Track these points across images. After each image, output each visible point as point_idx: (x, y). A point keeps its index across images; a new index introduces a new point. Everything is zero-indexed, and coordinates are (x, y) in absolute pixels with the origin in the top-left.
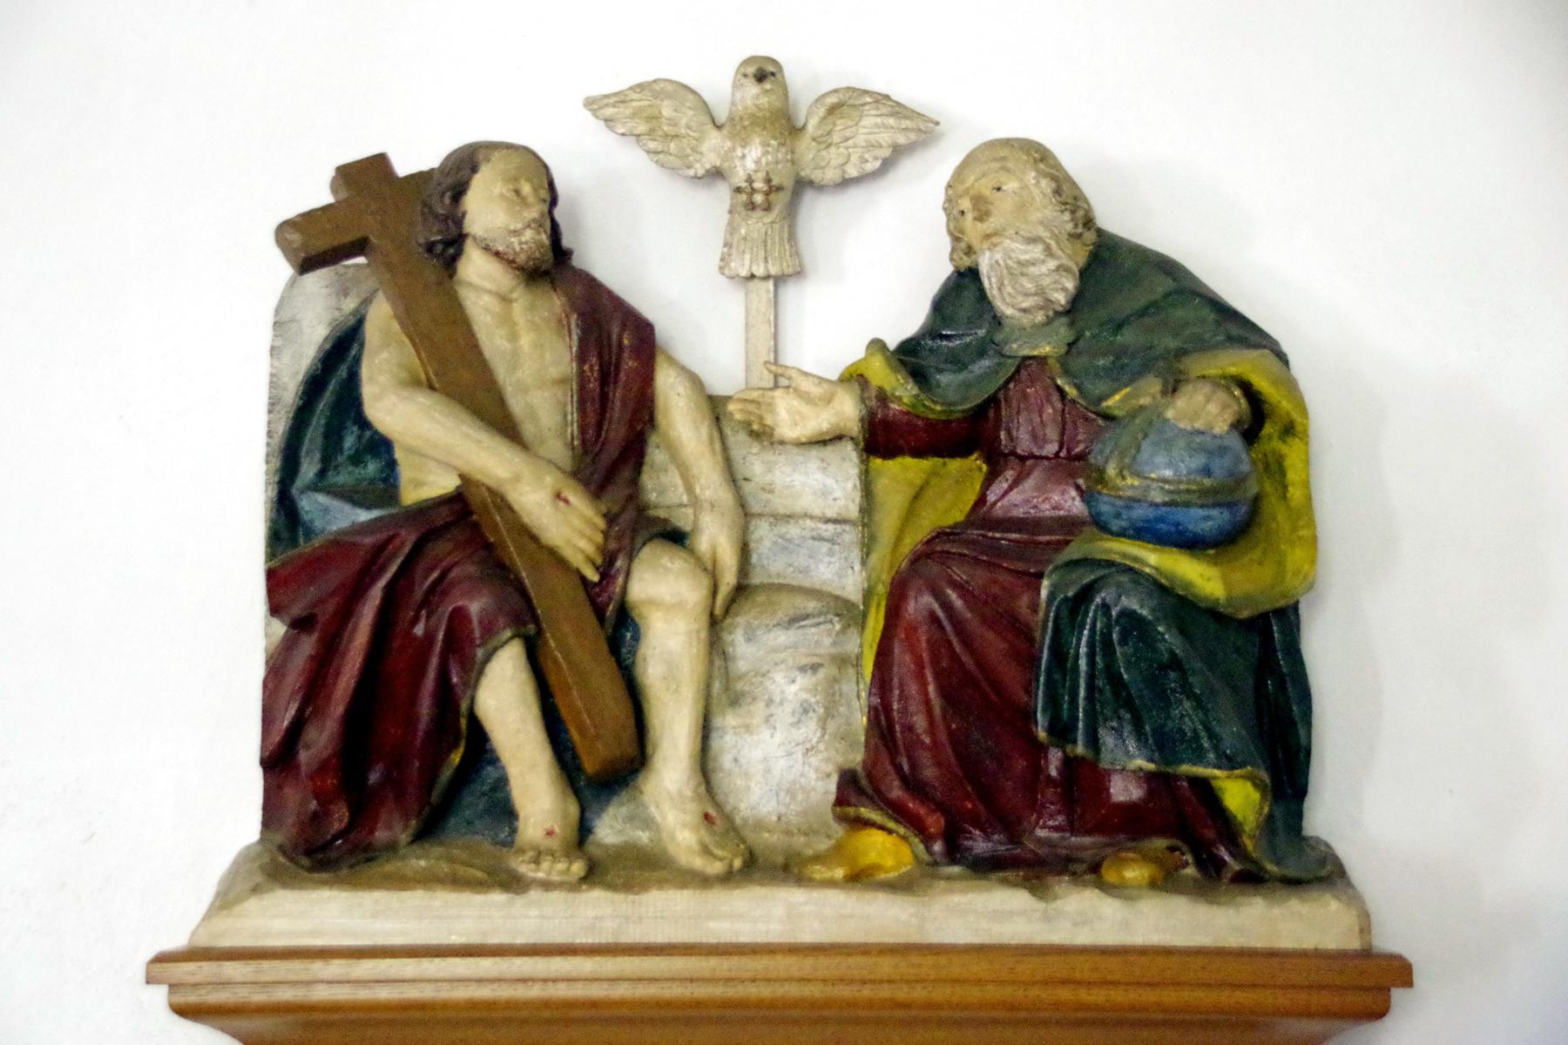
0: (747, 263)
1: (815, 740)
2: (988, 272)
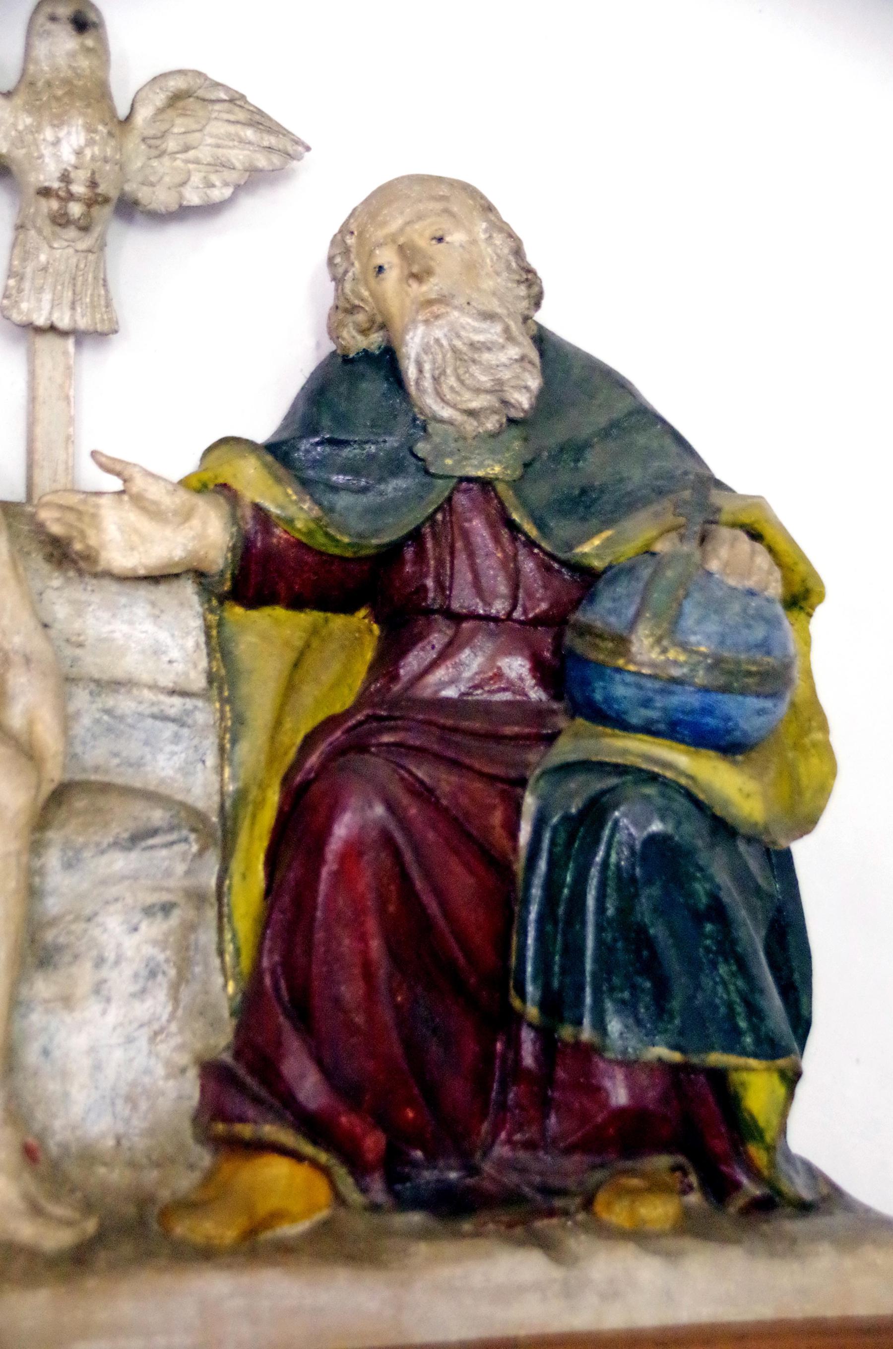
0: (46, 306)
1: (165, 1017)
2: (418, 355)
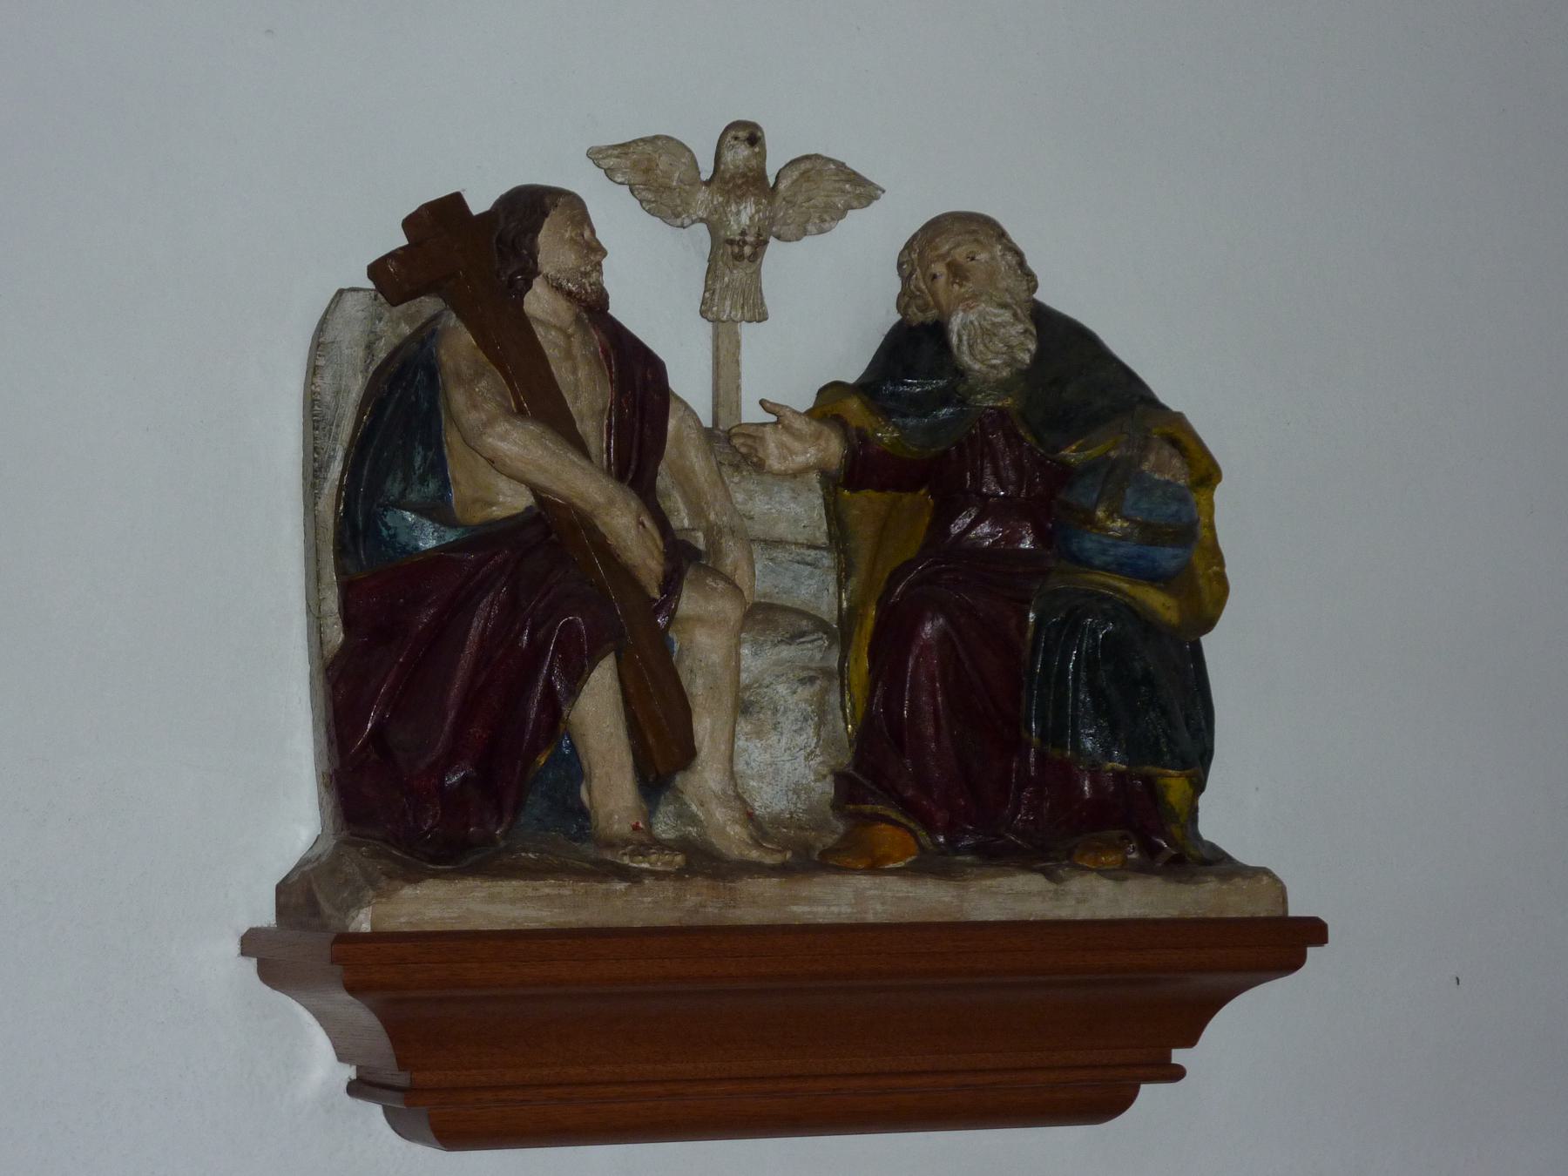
1: (813, 745)
